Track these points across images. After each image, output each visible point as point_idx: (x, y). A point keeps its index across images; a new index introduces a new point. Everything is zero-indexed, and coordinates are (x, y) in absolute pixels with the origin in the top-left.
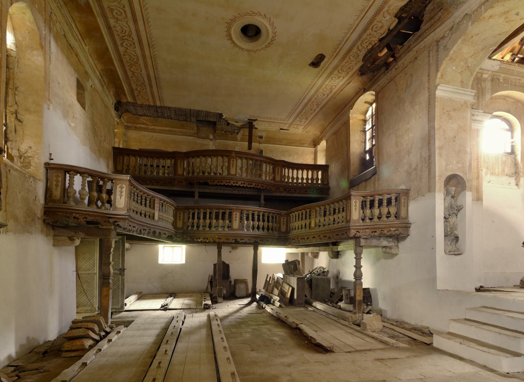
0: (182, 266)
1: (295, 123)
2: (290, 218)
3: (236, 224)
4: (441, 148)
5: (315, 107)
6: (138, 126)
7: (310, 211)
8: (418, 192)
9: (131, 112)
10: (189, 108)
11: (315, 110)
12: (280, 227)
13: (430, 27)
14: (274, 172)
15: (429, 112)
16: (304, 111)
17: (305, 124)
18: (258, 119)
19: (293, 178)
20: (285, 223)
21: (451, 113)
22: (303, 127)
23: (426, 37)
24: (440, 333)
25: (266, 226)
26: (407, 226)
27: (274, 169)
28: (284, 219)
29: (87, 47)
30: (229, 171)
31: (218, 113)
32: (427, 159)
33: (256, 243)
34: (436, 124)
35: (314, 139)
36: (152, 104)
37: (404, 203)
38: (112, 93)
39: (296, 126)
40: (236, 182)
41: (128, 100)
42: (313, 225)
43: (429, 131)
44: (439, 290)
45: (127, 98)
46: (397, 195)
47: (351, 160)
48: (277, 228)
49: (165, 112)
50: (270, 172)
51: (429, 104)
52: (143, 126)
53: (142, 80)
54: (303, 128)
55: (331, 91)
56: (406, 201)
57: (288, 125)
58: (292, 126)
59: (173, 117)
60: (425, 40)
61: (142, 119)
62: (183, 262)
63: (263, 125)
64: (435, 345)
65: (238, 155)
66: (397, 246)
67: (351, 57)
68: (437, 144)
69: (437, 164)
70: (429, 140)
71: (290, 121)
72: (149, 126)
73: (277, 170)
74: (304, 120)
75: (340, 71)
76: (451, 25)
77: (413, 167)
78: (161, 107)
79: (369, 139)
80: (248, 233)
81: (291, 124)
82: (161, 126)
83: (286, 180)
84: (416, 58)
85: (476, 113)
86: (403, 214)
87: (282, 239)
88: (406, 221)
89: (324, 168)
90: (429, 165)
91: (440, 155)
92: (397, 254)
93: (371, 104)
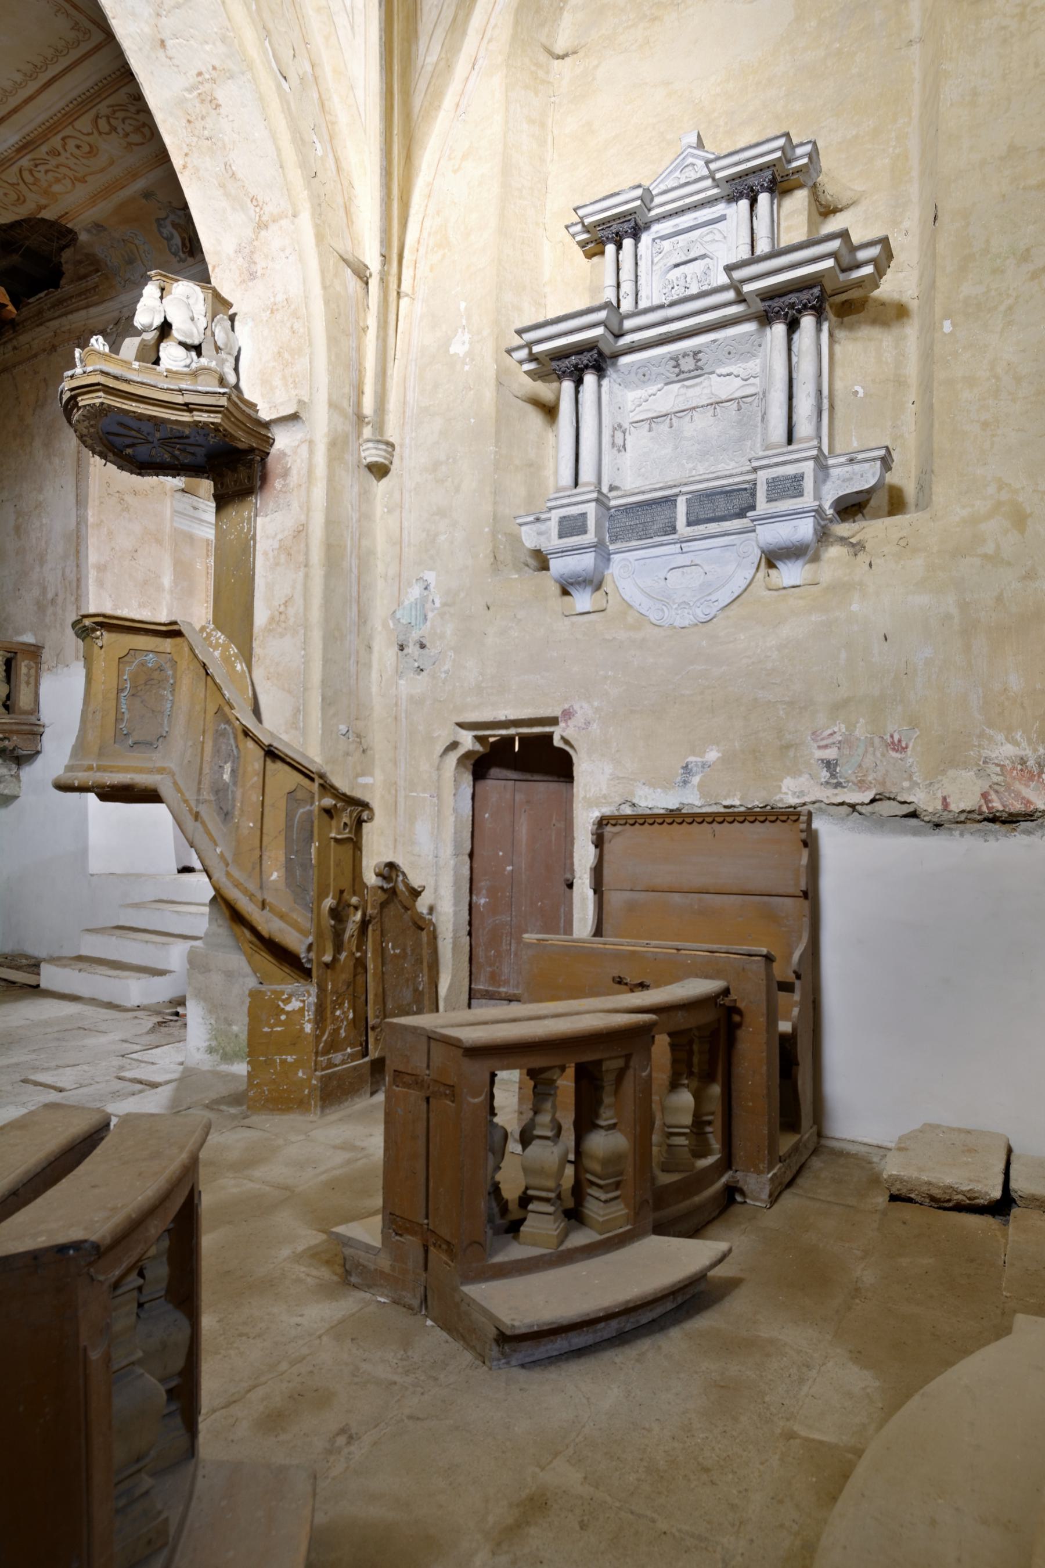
4: (101, 568)
8: (58, 655)
13: (80, 294)
15: (77, 481)
21: (126, 497)
23: (71, 312)
24: (53, 960)
26: (35, 732)
32: (74, 584)
34: (90, 513)
37: (28, 675)
43: (78, 524)
44: (92, 875)
46: (9, 655)
51: (78, 466)
56: (33, 671)
60: (70, 317)
64: (43, 985)
66: (17, 777)
68: (93, 557)
69: (91, 601)
70: (78, 544)
75: (103, 123)
76: (116, 314)
77: (50, 595)
84: (54, 348)
85: (202, 506)
86: (24, 700)
88: (33, 719)
90: (77, 599)
91: (101, 584)
92: (16, 797)
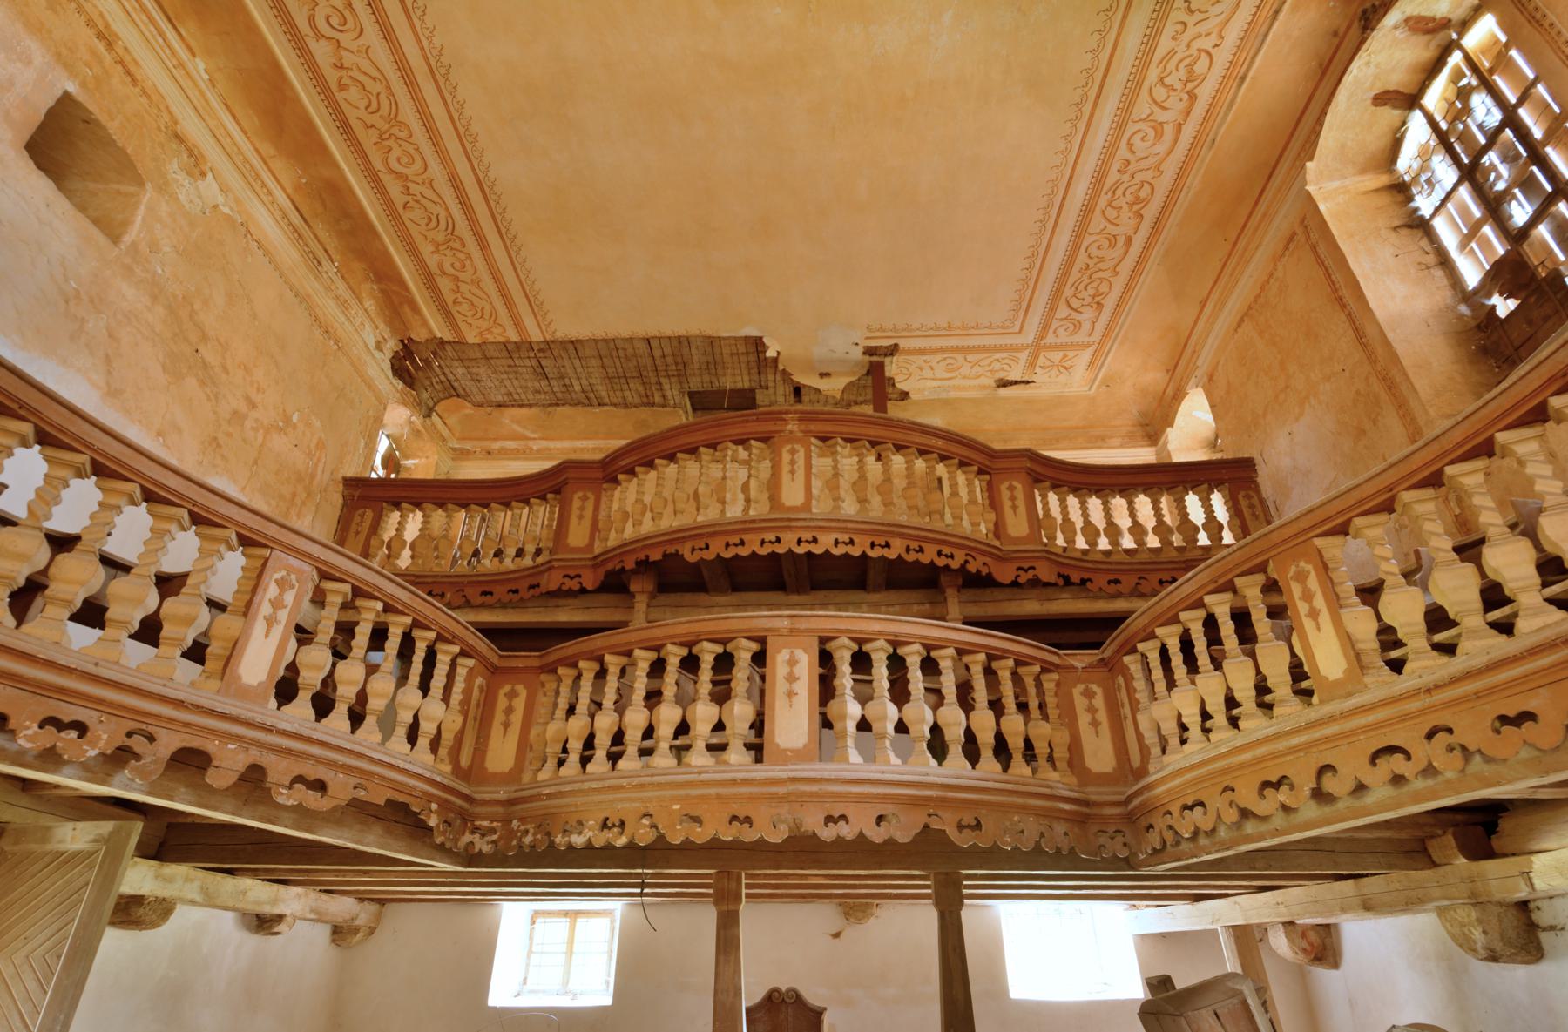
0: (1005, 991)
1: (1050, 339)
2: (1129, 679)
3: (792, 723)
5: (1126, 217)
6: (496, 445)
7: (1271, 587)
9: (466, 396)
10: (641, 333)
11: (1129, 241)
12: (1075, 747)
14: (994, 503)
16: (1082, 258)
17: (1096, 336)
18: (903, 344)
19: (1090, 531)
20: (1102, 716)
22: (1086, 355)
25: (986, 738)
27: (991, 489)
28: (1089, 694)
29: (201, 66)
30: (774, 499)
31: (746, 338)
33: (947, 861)
35: (1143, 414)
36: (514, 337)
38: (369, 304)
39: (1056, 356)
40: (807, 536)
41: (431, 331)
42: (1328, 660)
45: (425, 323)
47: (1400, 348)
48: (1061, 754)
49: (570, 372)
50: (972, 501)
52: (511, 444)
53: (443, 214)
54: (1091, 365)
55: (1193, 97)
57: (1023, 356)
58: (1041, 360)
59: (602, 390)
61: (509, 417)
62: (606, 1000)
63: (927, 373)
65: (812, 427)
67: (1094, 251)
71: (1029, 337)
72: (530, 443)
73: (1005, 494)
74: (1088, 314)
78: (548, 345)
79: (1464, 244)
80: (872, 772)
81: (1037, 348)
82: (571, 438)
83: (1060, 541)
87: (1103, 843)
89: (1231, 474)
93: (1411, 101)
